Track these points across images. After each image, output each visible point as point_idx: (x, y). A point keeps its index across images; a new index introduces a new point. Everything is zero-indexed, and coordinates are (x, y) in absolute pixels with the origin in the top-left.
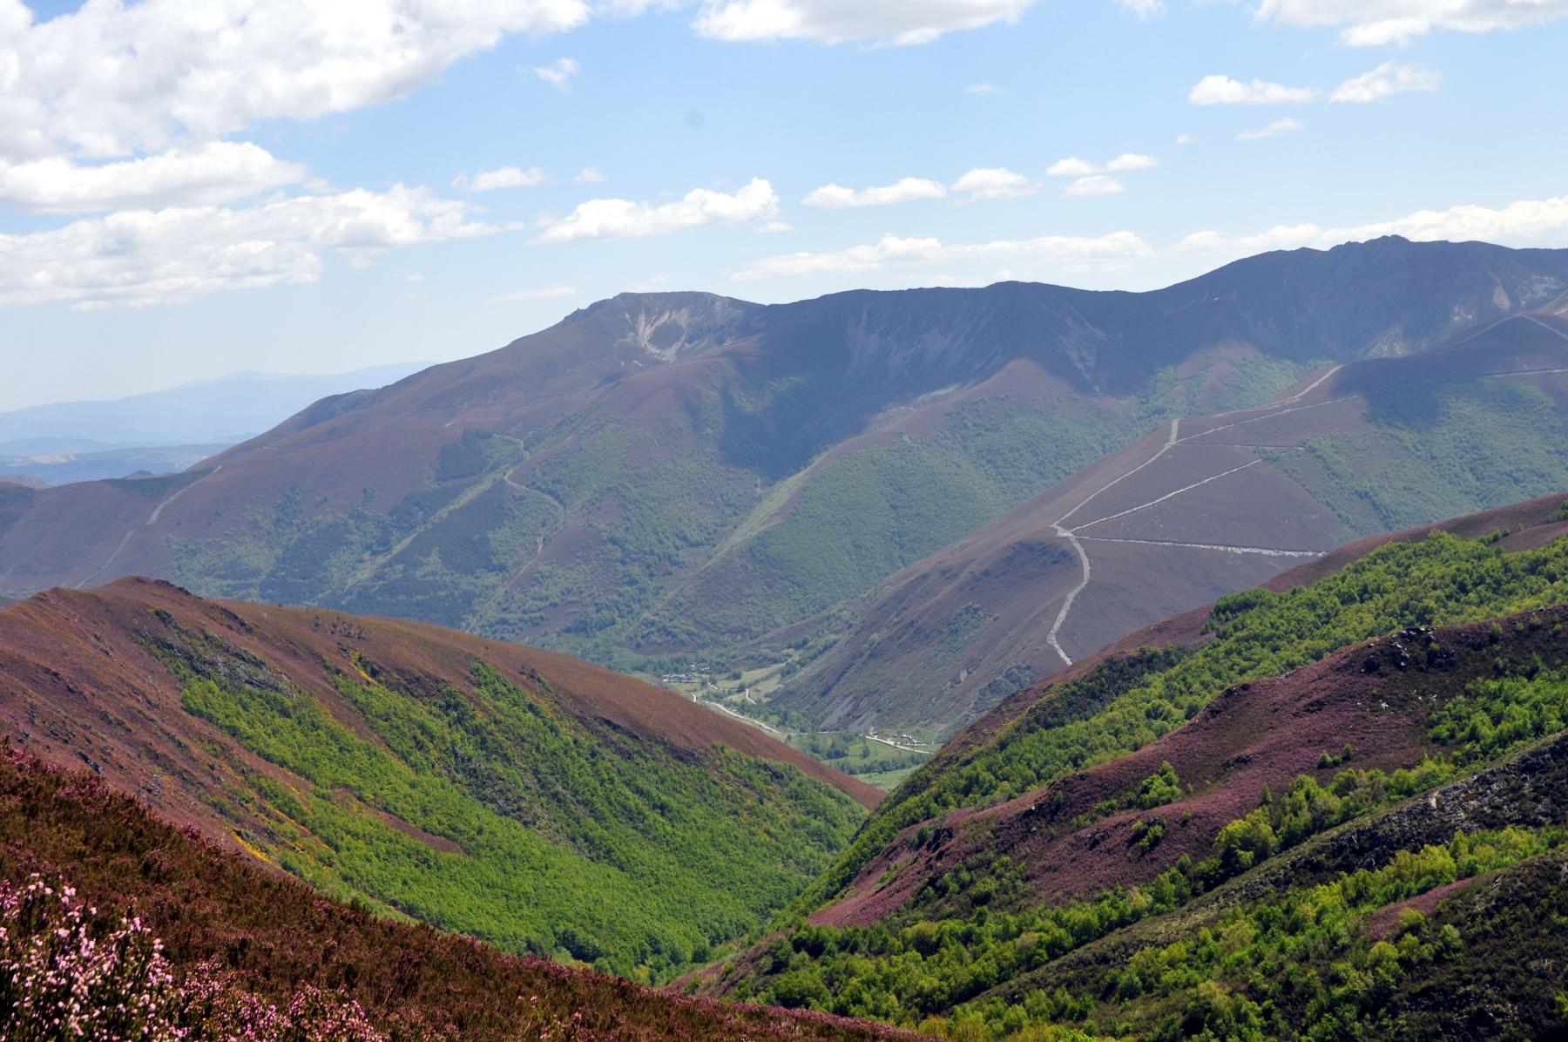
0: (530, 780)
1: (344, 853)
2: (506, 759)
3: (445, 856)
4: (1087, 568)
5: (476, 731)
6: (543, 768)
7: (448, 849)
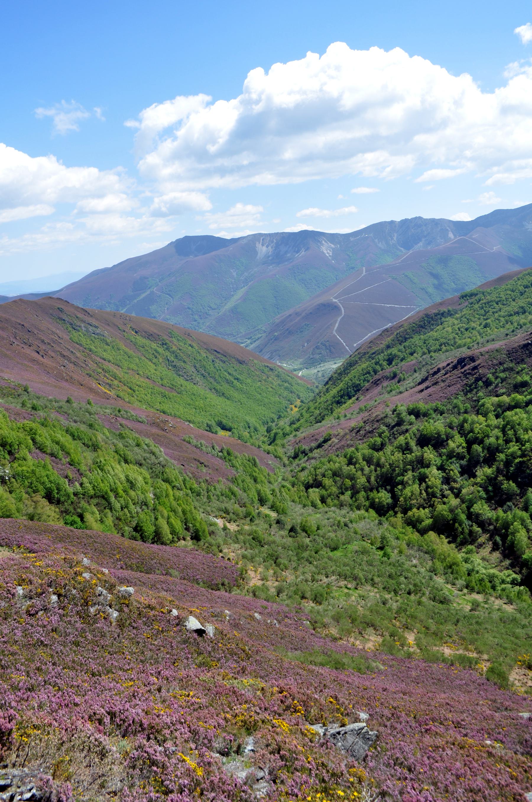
0: (194, 370)
1: (137, 392)
2: (184, 362)
3: (171, 395)
4: (343, 311)
5: (173, 352)
6: (197, 365)
7: (171, 392)
